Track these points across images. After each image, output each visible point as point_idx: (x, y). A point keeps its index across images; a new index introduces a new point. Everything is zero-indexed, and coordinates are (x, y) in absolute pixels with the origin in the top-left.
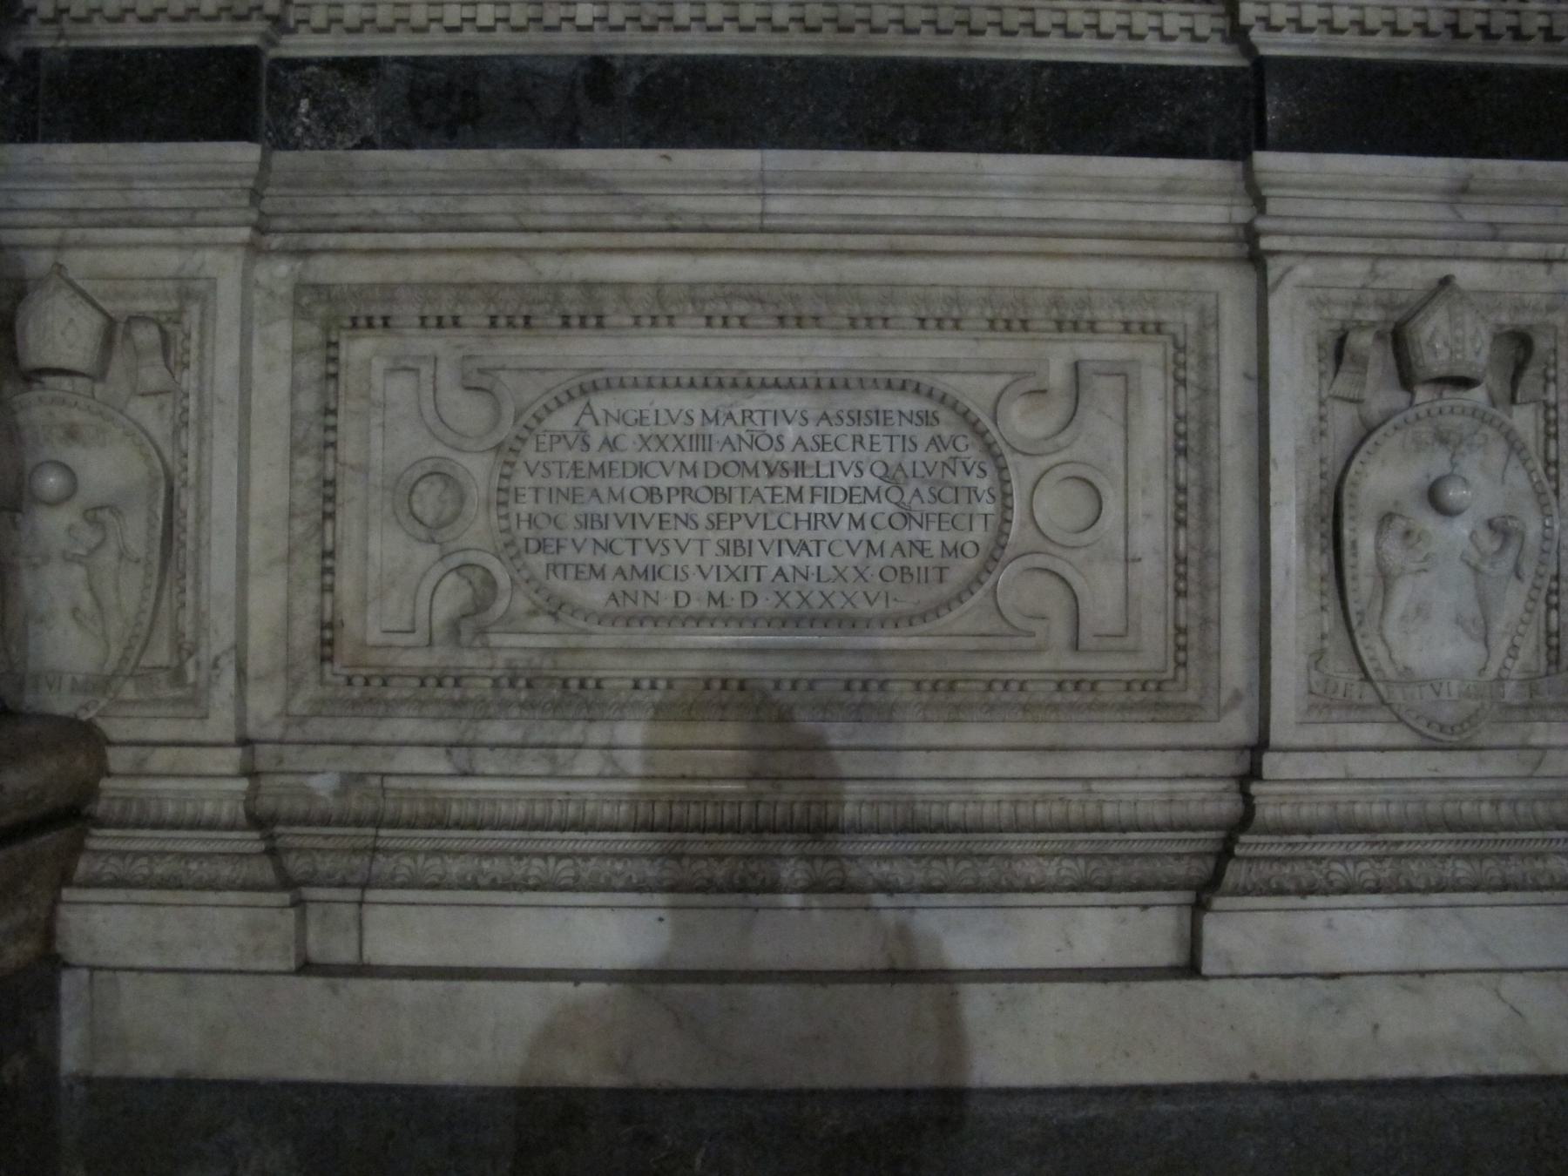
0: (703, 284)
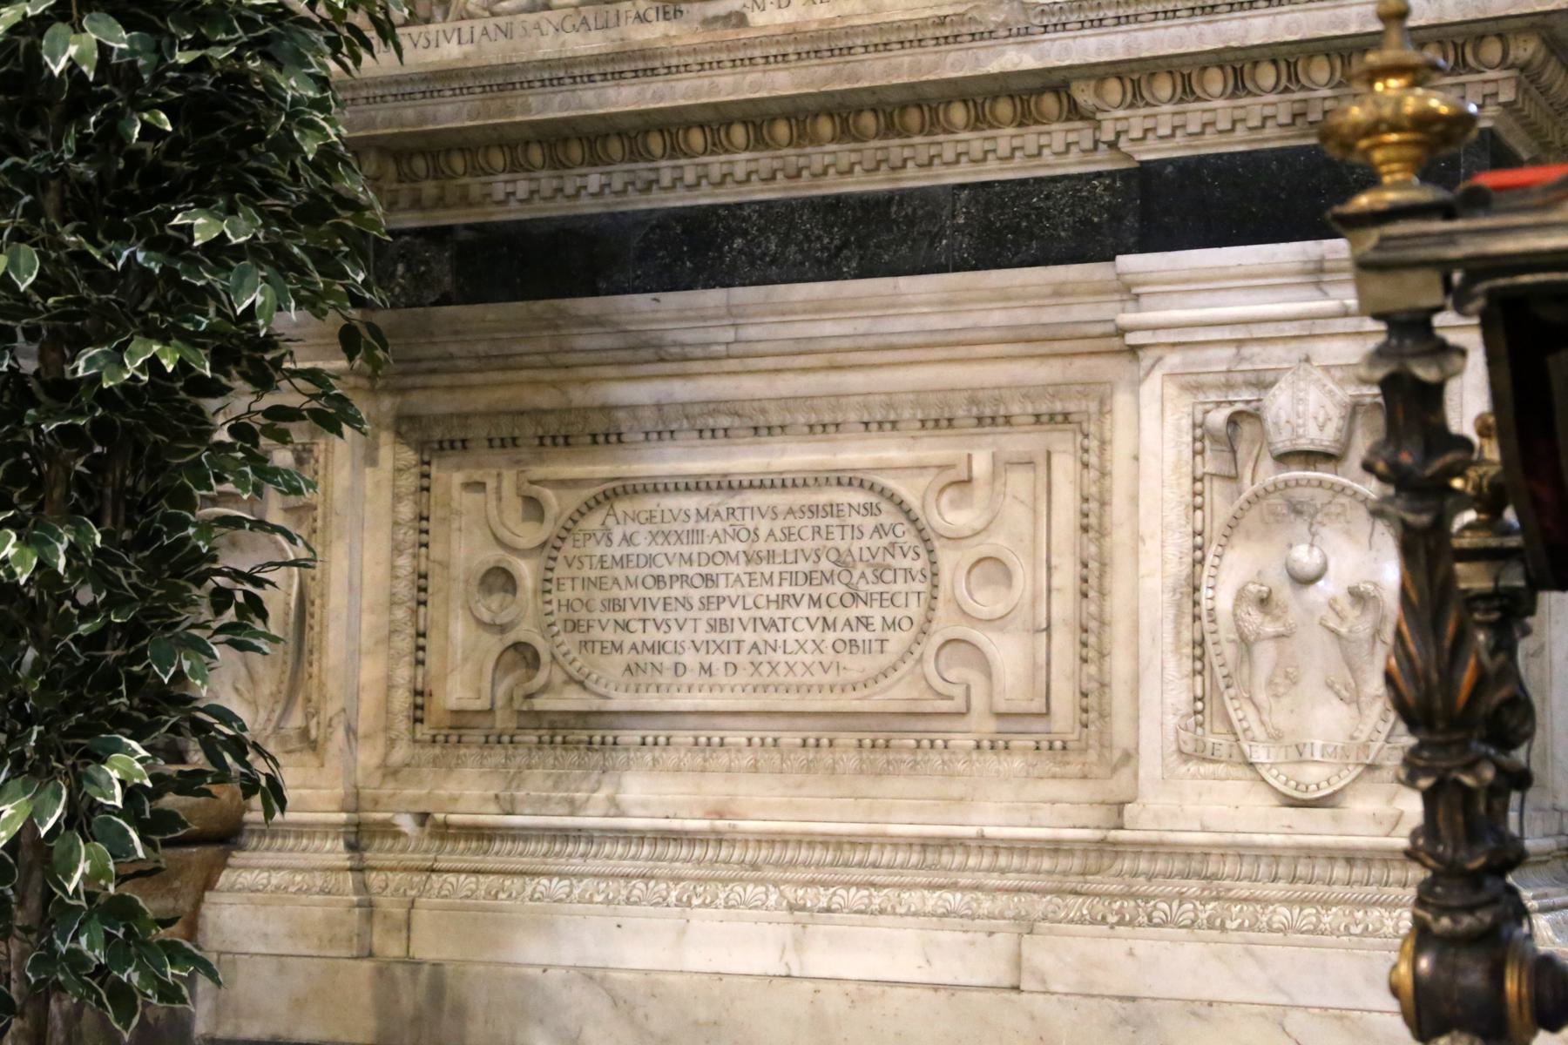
0: (692, 403)
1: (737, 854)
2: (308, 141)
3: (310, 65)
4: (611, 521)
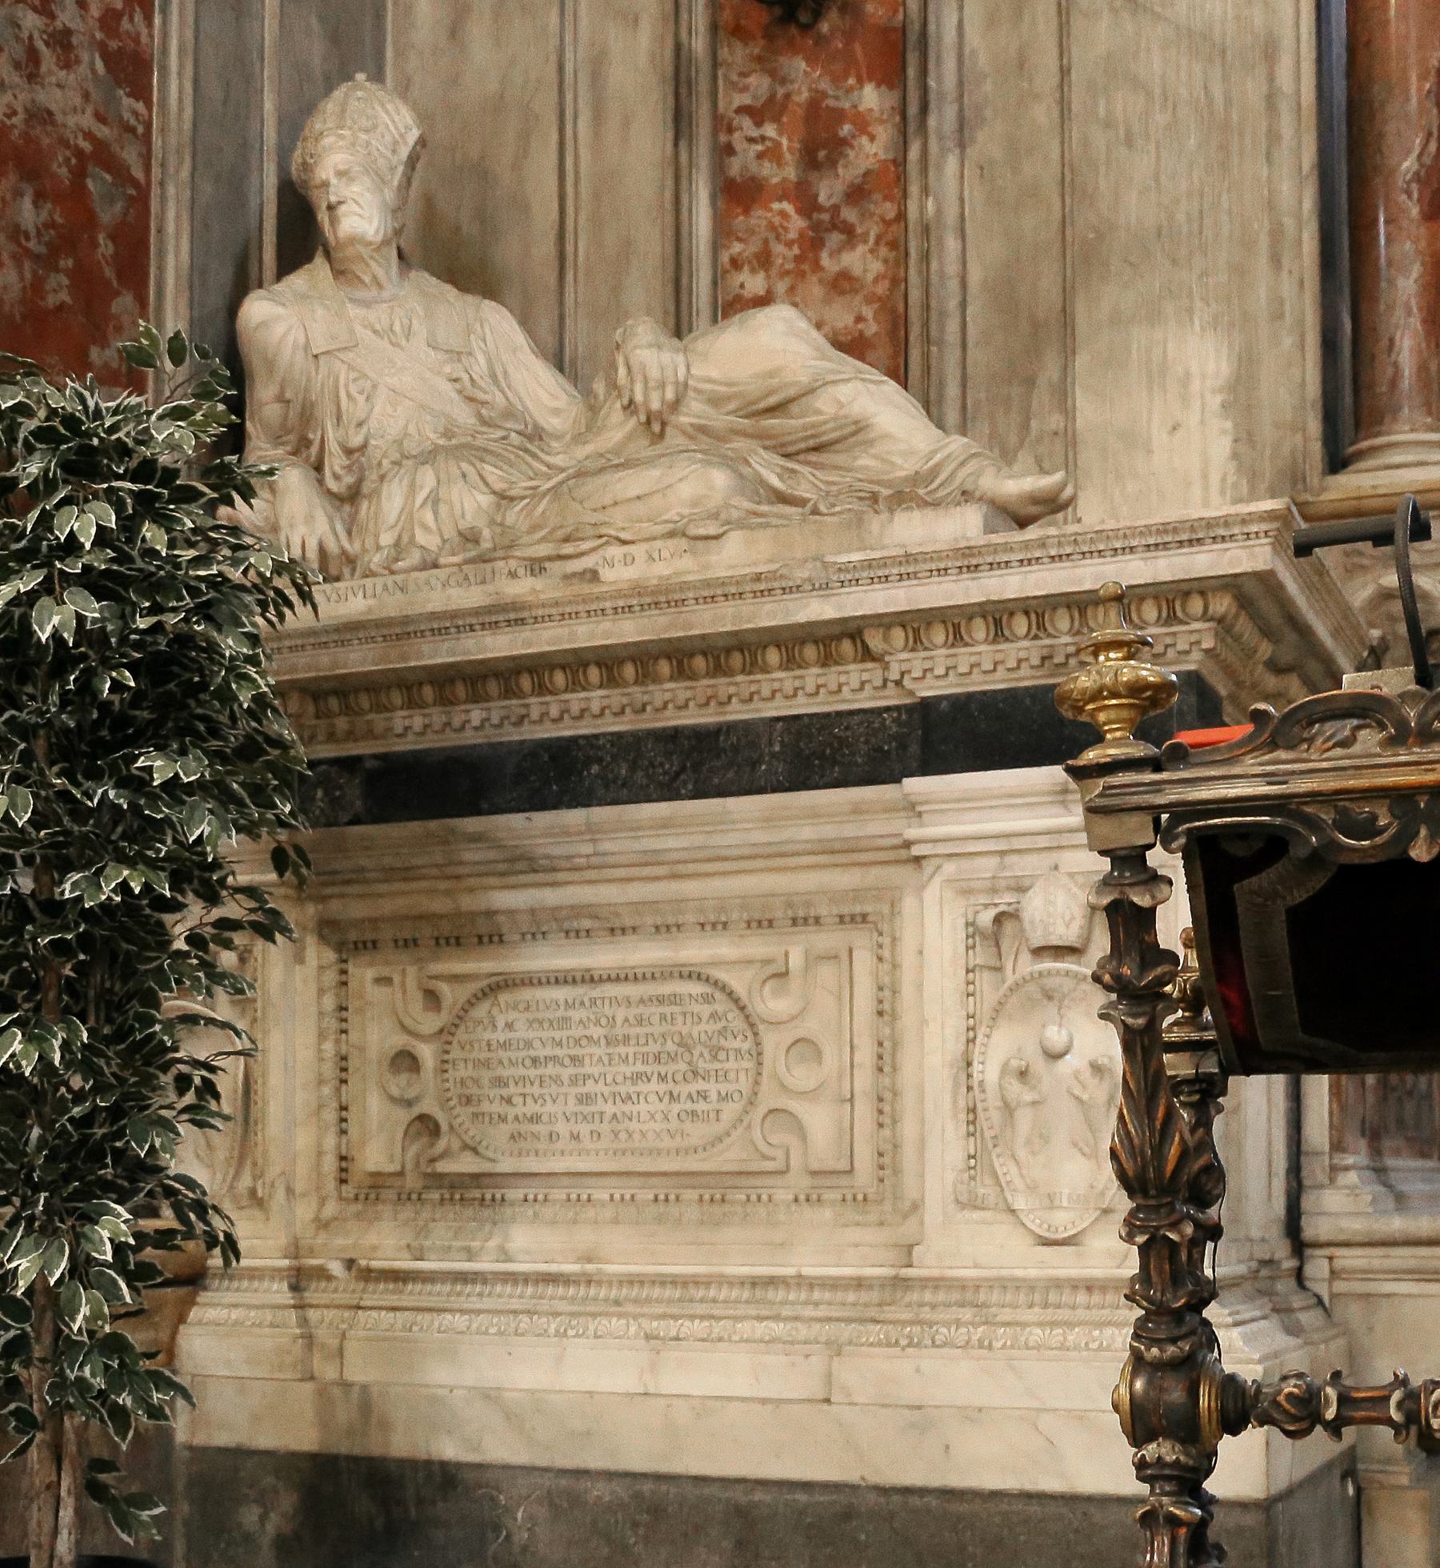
1: (603, 1293)
2: (244, 691)
3: (244, 626)
4: (495, 1010)
